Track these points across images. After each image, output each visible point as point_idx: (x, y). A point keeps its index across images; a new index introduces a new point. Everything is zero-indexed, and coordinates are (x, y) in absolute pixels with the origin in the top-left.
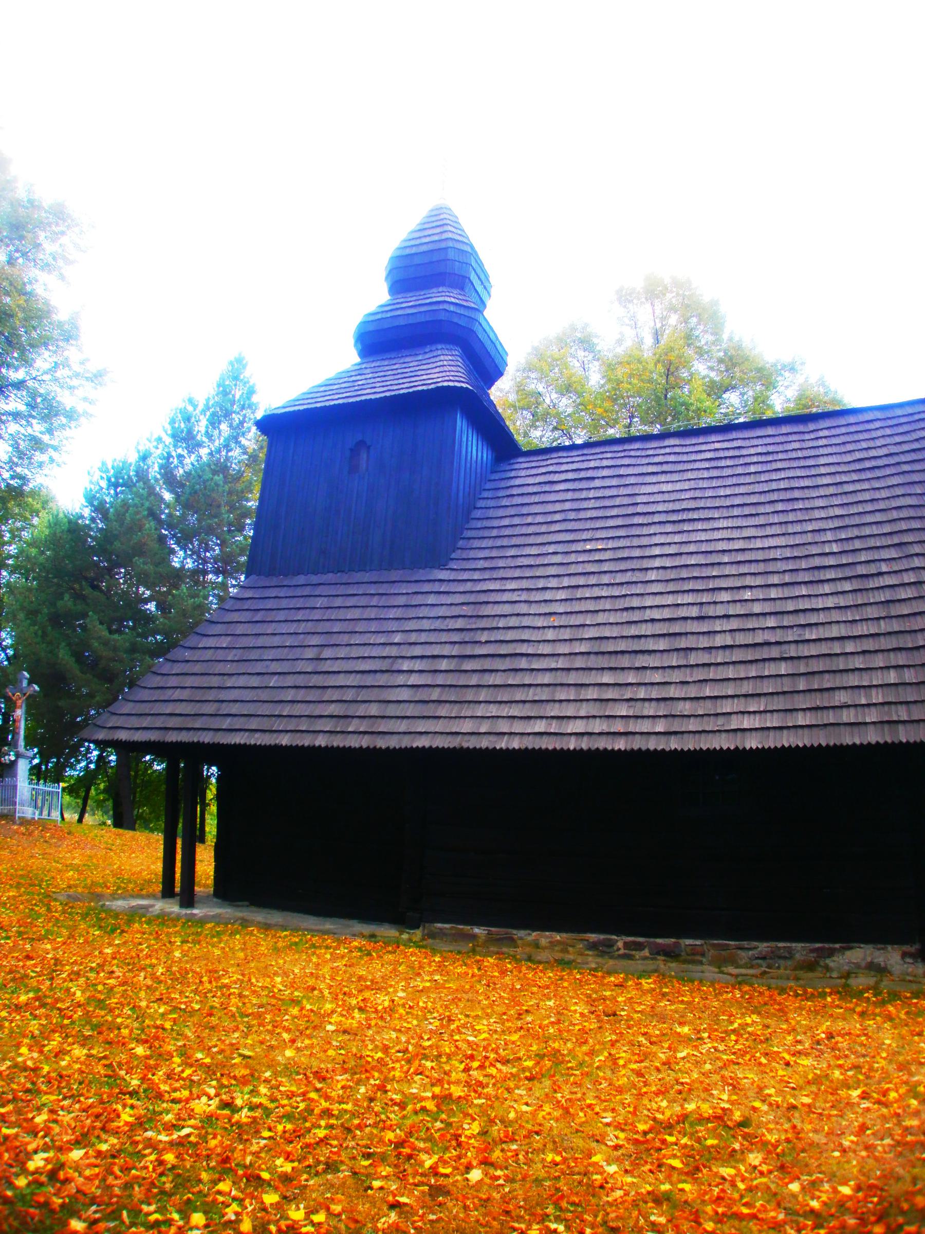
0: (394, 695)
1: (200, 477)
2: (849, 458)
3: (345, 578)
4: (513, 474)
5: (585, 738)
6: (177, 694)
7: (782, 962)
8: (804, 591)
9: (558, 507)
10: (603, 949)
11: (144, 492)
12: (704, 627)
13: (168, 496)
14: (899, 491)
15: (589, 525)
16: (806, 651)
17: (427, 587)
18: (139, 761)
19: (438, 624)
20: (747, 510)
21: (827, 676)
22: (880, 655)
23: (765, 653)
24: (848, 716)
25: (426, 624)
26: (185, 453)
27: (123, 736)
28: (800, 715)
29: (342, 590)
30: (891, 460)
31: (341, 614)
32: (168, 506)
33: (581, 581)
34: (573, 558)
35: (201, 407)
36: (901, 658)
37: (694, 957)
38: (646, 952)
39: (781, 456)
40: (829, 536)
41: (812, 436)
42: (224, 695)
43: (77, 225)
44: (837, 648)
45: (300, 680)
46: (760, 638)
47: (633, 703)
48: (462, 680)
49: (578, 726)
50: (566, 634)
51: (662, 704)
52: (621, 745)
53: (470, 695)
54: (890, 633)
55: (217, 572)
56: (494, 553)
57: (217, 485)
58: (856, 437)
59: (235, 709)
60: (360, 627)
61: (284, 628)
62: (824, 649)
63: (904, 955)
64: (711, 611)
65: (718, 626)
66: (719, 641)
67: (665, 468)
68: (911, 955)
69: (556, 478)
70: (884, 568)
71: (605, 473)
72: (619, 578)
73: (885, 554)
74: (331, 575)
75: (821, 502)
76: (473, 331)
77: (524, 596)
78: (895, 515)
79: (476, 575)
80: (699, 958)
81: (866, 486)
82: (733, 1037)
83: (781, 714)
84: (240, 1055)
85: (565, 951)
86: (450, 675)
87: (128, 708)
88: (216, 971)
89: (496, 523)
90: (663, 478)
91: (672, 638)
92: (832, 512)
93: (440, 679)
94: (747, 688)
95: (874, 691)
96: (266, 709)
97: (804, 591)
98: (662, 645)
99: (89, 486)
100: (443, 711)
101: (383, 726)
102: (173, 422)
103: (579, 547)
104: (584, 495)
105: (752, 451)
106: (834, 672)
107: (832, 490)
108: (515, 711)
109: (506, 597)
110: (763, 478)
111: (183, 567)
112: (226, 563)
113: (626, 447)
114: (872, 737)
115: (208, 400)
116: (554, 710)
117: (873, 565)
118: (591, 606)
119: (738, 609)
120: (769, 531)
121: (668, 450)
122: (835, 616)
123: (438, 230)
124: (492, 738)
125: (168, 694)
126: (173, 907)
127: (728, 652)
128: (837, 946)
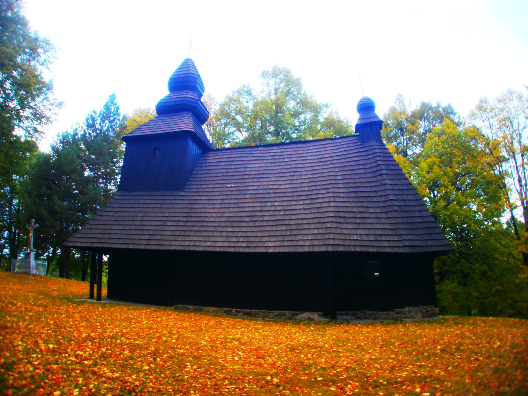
2: (317, 157)
3: (151, 193)
4: (207, 158)
6: (96, 231)
7: (283, 317)
8: (294, 203)
9: (221, 171)
12: (261, 214)
14: (330, 170)
15: (230, 178)
16: (291, 222)
17: (177, 198)
20: (281, 175)
23: (279, 223)
24: (300, 243)
25: (176, 210)
27: (78, 245)
30: (331, 159)
31: (150, 206)
33: (225, 197)
34: (224, 189)
36: (319, 226)
38: (242, 314)
39: (295, 156)
40: (305, 185)
41: (307, 149)
43: (54, 49)
44: (301, 222)
45: (136, 227)
48: (186, 229)
49: (220, 244)
50: (219, 215)
51: (245, 238)
52: (232, 250)
53: (188, 234)
56: (199, 187)
57: (104, 146)
59: (115, 236)
60: (155, 210)
61: (130, 210)
63: (319, 315)
64: (264, 209)
65: (266, 214)
66: (265, 218)
67: (257, 158)
69: (222, 160)
70: (320, 196)
71: (237, 159)
72: (238, 197)
73: (321, 192)
75: (305, 173)
76: (196, 108)
77: (207, 202)
78: (327, 178)
79: (193, 194)
81: (321, 168)
86: (183, 227)
90: (256, 162)
93: (179, 228)
94: (272, 234)
97: (294, 203)
98: (248, 219)
99: (52, 142)
100: (180, 238)
102: (87, 120)
105: (287, 153)
107: (309, 169)
108: (201, 239)
110: (288, 163)
113: (246, 150)
114: (306, 249)
116: (213, 239)
118: (227, 206)
119: (273, 209)
120: (287, 182)
122: (302, 212)
123: (187, 69)
124: (194, 247)
125: (93, 231)
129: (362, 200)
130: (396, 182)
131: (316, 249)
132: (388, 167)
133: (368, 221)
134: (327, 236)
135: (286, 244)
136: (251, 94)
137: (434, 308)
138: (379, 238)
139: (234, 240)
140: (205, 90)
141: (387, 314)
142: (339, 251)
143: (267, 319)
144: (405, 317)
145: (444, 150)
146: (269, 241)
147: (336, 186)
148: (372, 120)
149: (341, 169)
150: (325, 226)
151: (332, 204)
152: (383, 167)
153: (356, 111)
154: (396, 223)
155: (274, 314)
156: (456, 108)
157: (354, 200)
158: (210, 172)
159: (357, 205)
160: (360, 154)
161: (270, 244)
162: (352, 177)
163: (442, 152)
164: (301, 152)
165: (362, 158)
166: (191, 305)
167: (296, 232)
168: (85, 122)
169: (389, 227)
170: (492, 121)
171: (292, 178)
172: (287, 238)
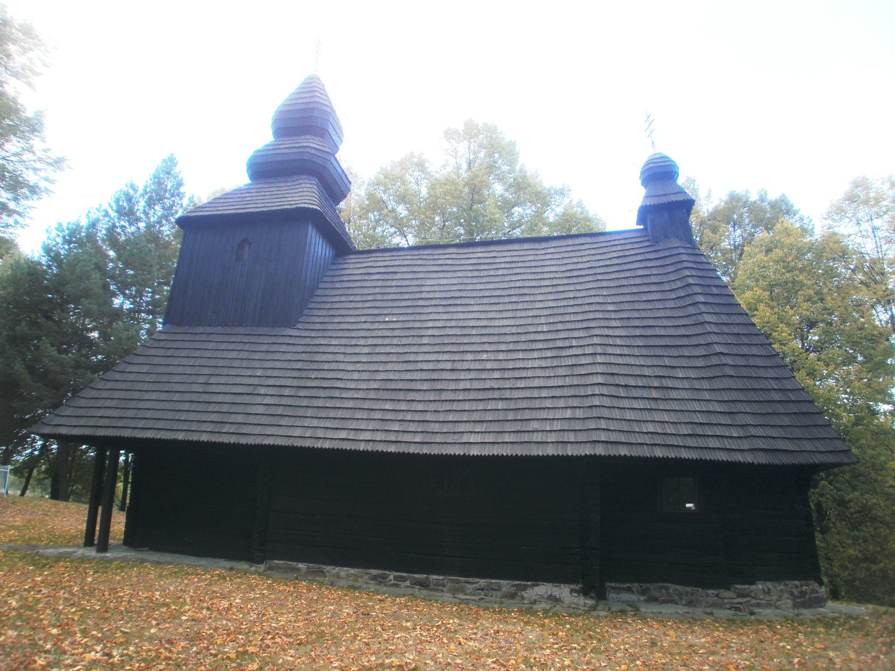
0: (253, 410)
1: (137, 244)
2: (564, 268)
3: (228, 330)
4: (345, 266)
5: (371, 443)
6: (108, 403)
7: (494, 592)
8: (521, 355)
9: (371, 291)
10: (380, 580)
11: (93, 251)
12: (454, 376)
13: (112, 254)
14: (592, 293)
17: (281, 340)
18: (76, 449)
19: (285, 365)
20: (493, 300)
21: (527, 411)
22: (563, 400)
23: (490, 395)
24: (537, 437)
25: (278, 365)
26: (126, 224)
27: (64, 431)
28: (507, 435)
29: (226, 338)
31: (225, 355)
32: (112, 261)
33: (379, 341)
34: (376, 326)
35: (140, 192)
36: (576, 402)
37: (438, 587)
38: (408, 583)
39: (520, 265)
40: (543, 320)
41: (543, 252)
42: (141, 405)
45: (195, 397)
46: (488, 384)
47: (402, 423)
48: (297, 402)
49: (367, 436)
50: (365, 376)
51: (421, 424)
52: (392, 449)
53: (301, 412)
54: (571, 386)
55: (148, 312)
57: (150, 251)
58: (571, 255)
59: (148, 414)
62: (528, 394)
63: (572, 591)
64: (459, 366)
65: (462, 376)
66: (462, 385)
67: (444, 268)
70: (574, 343)
71: (405, 269)
73: (576, 334)
74: (219, 328)
77: (342, 350)
78: (587, 308)
79: (313, 334)
80: (440, 587)
81: (572, 288)
82: (435, 629)
83: (494, 434)
84: (121, 631)
85: (356, 580)
87: (69, 411)
88: (116, 589)
89: (330, 299)
90: (441, 275)
91: (432, 383)
92: (547, 304)
93: (284, 401)
94: (476, 417)
95: (555, 422)
96: (170, 415)
97: (521, 355)
98: (425, 386)
100: (284, 421)
101: (245, 430)
102: (117, 201)
103: (381, 319)
104: (389, 283)
105: (503, 260)
106: (532, 409)
107: (550, 289)
108: (328, 424)
109: (331, 349)
110: (506, 279)
111: (121, 307)
112: (155, 307)
114: (550, 451)
115: (146, 187)
116: (353, 425)
117: (567, 341)
119: (478, 366)
120: (505, 315)
121: (447, 256)
124: (313, 440)
125: (100, 403)
126: (92, 552)
127: (467, 393)
128: (529, 583)
129: (659, 352)
130: (725, 319)
131: (570, 451)
132: (707, 290)
133: (674, 394)
134: (592, 425)
135: (507, 438)
136: (426, 169)
137: (816, 586)
138: (699, 431)
139: (396, 427)
140: (344, 140)
141: (717, 595)
142: (620, 455)
143: (461, 596)
144: (758, 605)
145: (778, 276)
146: (471, 432)
147: (606, 323)
148: (674, 198)
149: (613, 292)
150: (588, 402)
151: (599, 359)
152: (698, 290)
153: (640, 182)
154: (733, 401)
155: (477, 585)
156: (796, 202)
157: (644, 352)
158: (350, 292)
159: (649, 362)
160: (649, 264)
161: (473, 438)
162: (637, 306)
163: (775, 280)
164: (532, 258)
165: (655, 271)
166: (302, 561)
167: (527, 415)
168: (113, 204)
169: (718, 408)
170: (877, 222)
171: (515, 307)
172: (509, 427)
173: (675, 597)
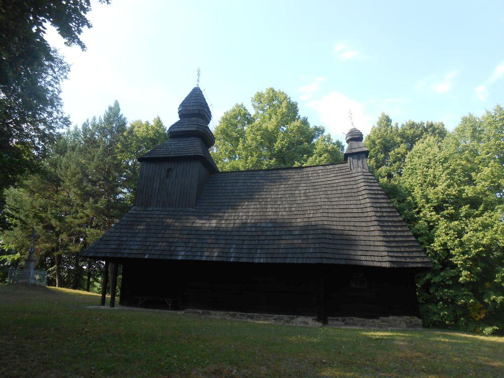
38: (245, 317)
63: (313, 319)
68: (314, 320)
141: (373, 322)
166: (200, 309)
173: (356, 323)
